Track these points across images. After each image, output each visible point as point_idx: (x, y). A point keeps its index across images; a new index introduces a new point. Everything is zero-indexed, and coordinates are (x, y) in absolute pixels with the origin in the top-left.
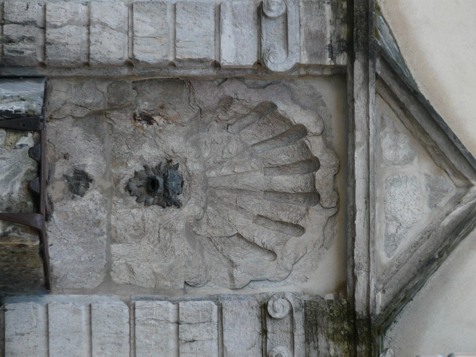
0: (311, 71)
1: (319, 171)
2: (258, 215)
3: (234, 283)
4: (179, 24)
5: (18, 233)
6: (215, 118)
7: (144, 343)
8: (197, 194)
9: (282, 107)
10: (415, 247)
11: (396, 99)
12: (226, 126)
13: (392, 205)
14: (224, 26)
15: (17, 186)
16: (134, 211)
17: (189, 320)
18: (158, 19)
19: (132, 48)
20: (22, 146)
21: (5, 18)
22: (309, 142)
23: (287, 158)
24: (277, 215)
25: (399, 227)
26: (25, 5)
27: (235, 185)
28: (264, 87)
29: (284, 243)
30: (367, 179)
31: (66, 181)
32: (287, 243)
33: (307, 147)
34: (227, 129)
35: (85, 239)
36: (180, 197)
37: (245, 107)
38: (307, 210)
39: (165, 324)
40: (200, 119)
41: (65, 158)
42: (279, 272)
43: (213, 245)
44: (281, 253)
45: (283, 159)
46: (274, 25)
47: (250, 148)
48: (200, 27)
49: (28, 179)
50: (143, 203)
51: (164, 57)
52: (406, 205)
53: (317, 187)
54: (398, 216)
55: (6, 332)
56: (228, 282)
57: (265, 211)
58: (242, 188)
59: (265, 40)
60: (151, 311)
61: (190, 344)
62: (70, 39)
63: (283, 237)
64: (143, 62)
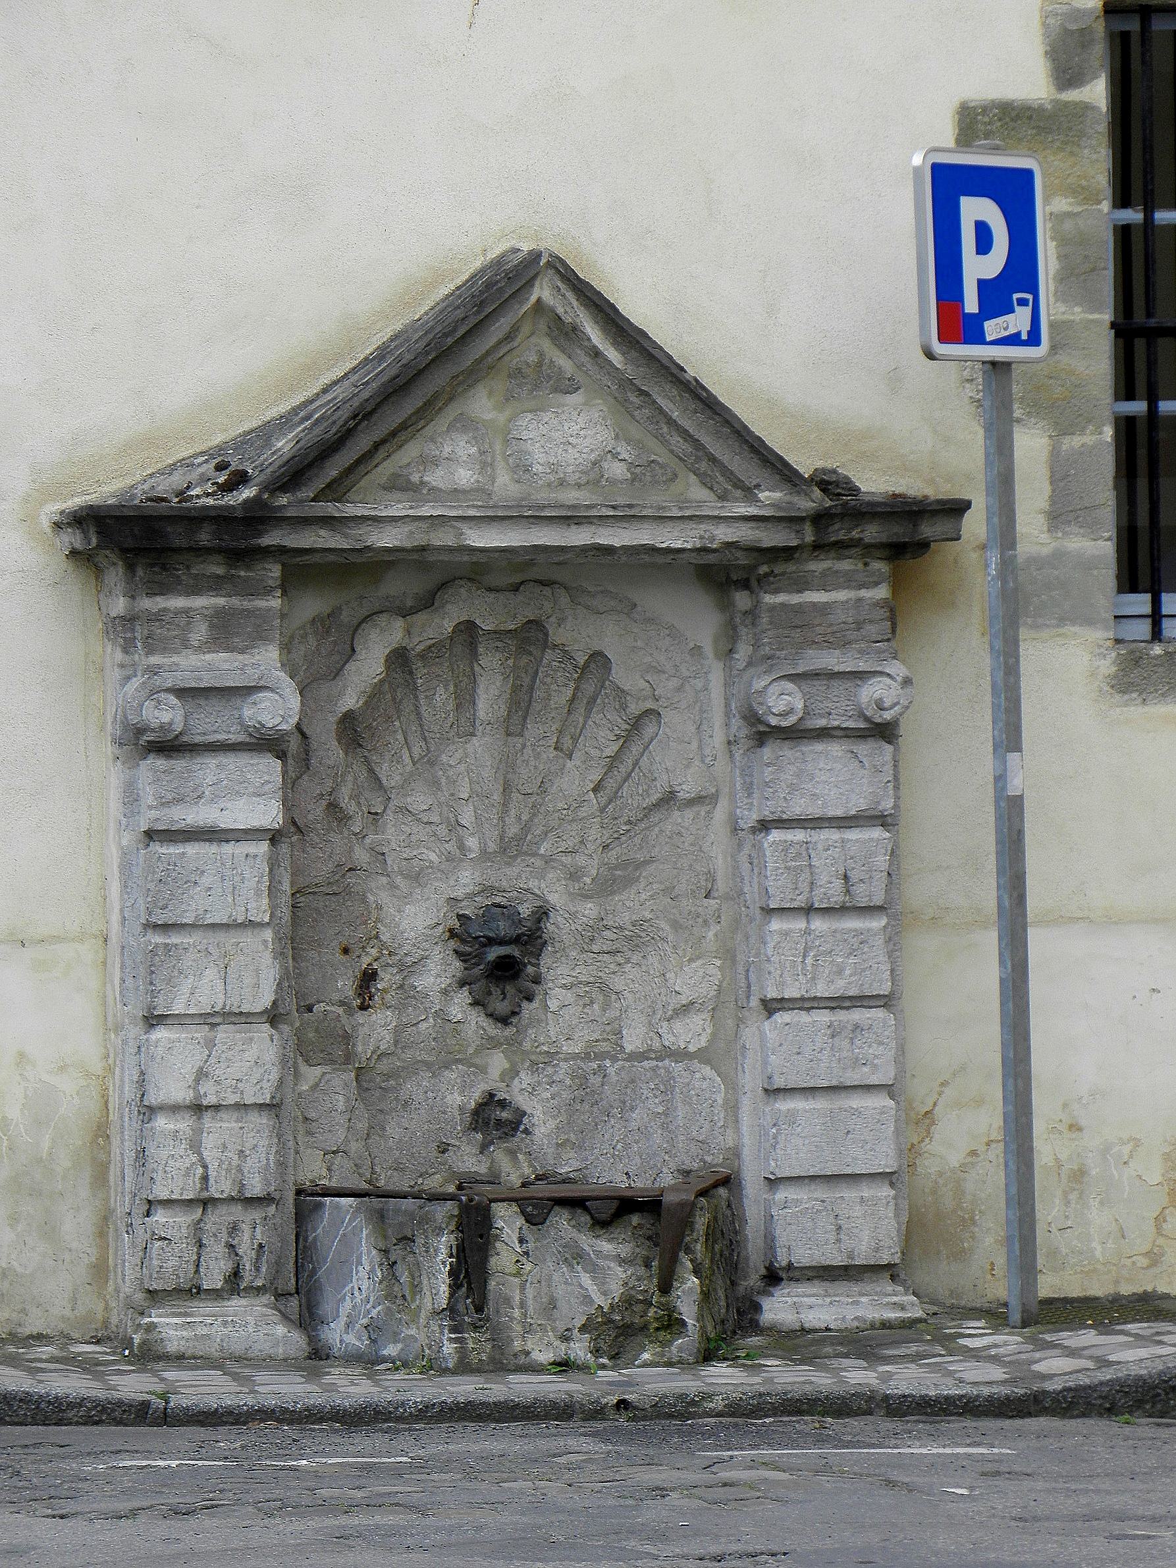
3: (705, 797)
5: (696, 1241)
8: (519, 876)
9: (350, 701)
15: (606, 1246)
16: (553, 1005)
17: (804, 886)
18: (188, 960)
19: (249, 1014)
20: (522, 1241)
22: (421, 644)
23: (441, 690)
24: (557, 708)
25: (615, 456)
27: (497, 797)
29: (620, 692)
34: (376, 814)
36: (525, 910)
40: (364, 870)
42: (683, 704)
43: (617, 842)
44: (645, 699)
46: (198, 717)
51: (267, 947)
52: (570, 441)
53: (512, 627)
54: (593, 457)
56: (703, 810)
57: (548, 735)
59: (231, 736)
60: (788, 965)
61: (852, 885)
64: (276, 993)
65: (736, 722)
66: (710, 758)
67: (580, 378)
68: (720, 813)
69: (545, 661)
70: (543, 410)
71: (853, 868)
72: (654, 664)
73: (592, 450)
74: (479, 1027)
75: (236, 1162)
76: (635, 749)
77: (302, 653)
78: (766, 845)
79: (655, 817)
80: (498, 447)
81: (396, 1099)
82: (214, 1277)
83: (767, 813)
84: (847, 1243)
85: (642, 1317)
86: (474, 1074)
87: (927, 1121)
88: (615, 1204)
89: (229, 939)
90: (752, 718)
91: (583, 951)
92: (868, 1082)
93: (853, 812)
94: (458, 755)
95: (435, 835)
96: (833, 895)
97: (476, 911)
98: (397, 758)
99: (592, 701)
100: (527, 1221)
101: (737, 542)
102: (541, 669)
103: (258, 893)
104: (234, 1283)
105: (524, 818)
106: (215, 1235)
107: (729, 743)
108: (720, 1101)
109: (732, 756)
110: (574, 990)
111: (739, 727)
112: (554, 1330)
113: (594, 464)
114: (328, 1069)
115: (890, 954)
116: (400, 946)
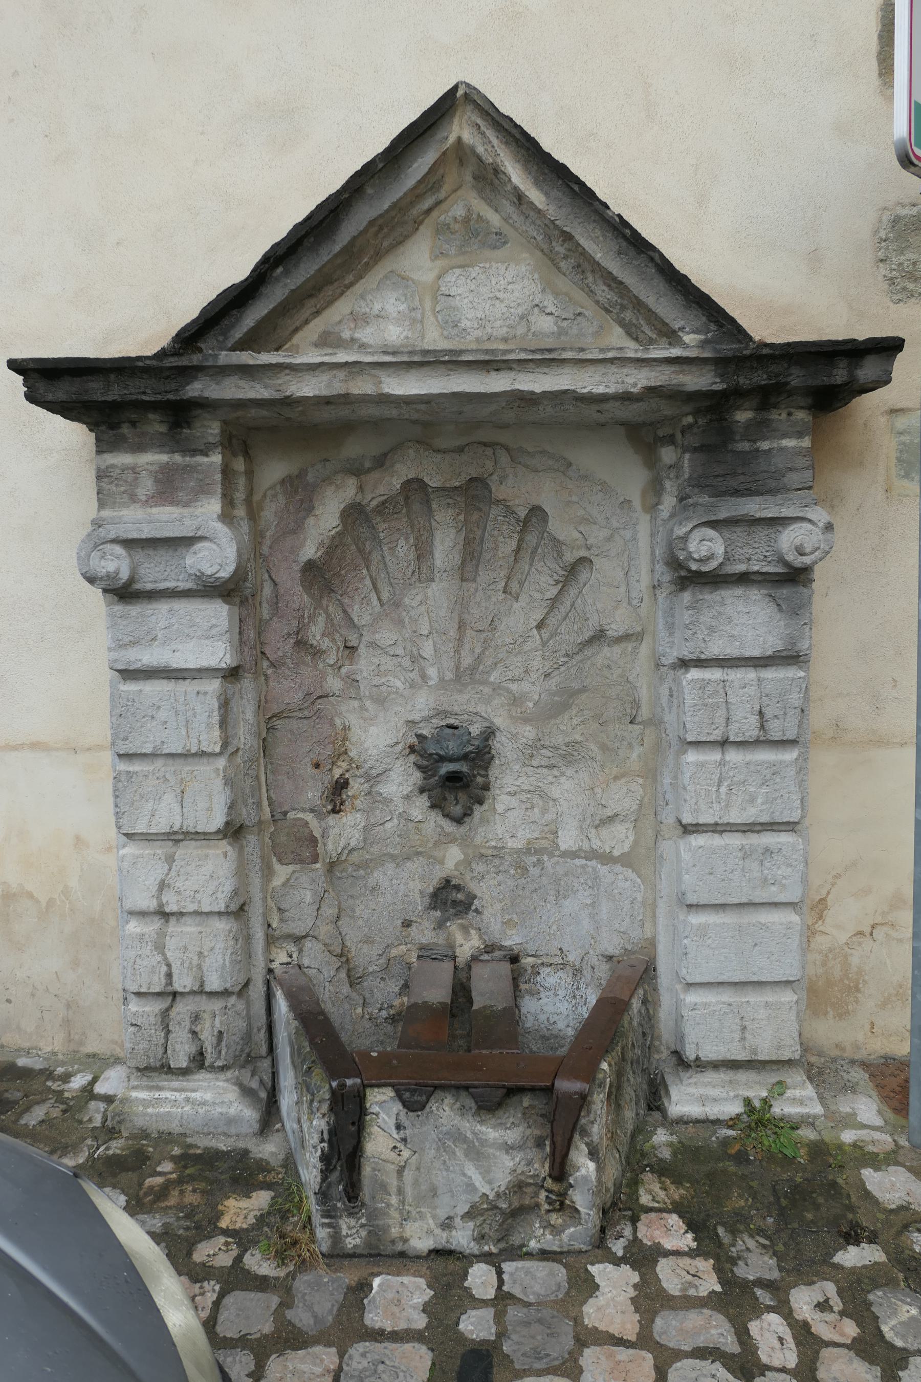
0: (694, 829)
1: (426, 479)
2: (504, 592)
3: (632, 635)
4: (154, 748)
6: (334, 670)
7: (764, 807)
9: (310, 551)
10: (583, 272)
11: (285, 309)
12: (347, 651)
13: (498, 323)
14: (155, 663)
16: (500, 808)
17: (721, 721)
19: (205, 834)
20: (399, 1127)
21: (158, 1064)
23: (402, 542)
24: (504, 557)
26: (132, 1029)
27: (453, 633)
28: (275, 584)
29: (557, 543)
30: (450, 366)
31: (448, 924)
32: (561, 539)
33: (383, 503)
35: (551, 892)
37: (312, 618)
38: (498, 502)
39: (727, 767)
41: (408, 926)
44: (579, 548)
45: (405, 548)
47: (386, 607)
48: (159, 707)
49: (473, 1111)
50: (485, 793)
52: (498, 296)
53: (457, 484)
54: (520, 311)
55: (739, 1058)
56: (630, 646)
58: (457, 621)
59: (179, 584)
60: (703, 793)
62: (190, 948)
63: (546, 546)
65: (660, 567)
66: (637, 601)
67: (507, 230)
68: (644, 649)
69: (491, 516)
70: (472, 265)
71: (768, 706)
72: (586, 517)
73: (519, 304)
74: (438, 825)
75: (195, 962)
76: (573, 592)
77: (273, 510)
78: (684, 683)
79: (588, 652)
80: (428, 304)
81: (365, 886)
82: (180, 1057)
83: (686, 653)
84: (751, 1040)
85: (532, 1198)
86: (433, 864)
87: (820, 906)
88: (505, 1091)
89: (186, 768)
90: (674, 563)
91: (524, 765)
92: (776, 900)
93: (769, 653)
94: (419, 598)
95: (400, 665)
96: (748, 730)
97: (433, 731)
98: (365, 600)
99: (534, 552)
100: (404, 1106)
101: (661, 386)
102: (489, 523)
103: (209, 726)
104: (199, 1061)
105: (478, 650)
106: (179, 1023)
107: (654, 587)
108: (640, 899)
109: (656, 599)
110: (518, 796)
111: (666, 576)
112: (434, 1217)
113: (522, 317)
114: (298, 867)
115: (801, 784)
116: (365, 761)
